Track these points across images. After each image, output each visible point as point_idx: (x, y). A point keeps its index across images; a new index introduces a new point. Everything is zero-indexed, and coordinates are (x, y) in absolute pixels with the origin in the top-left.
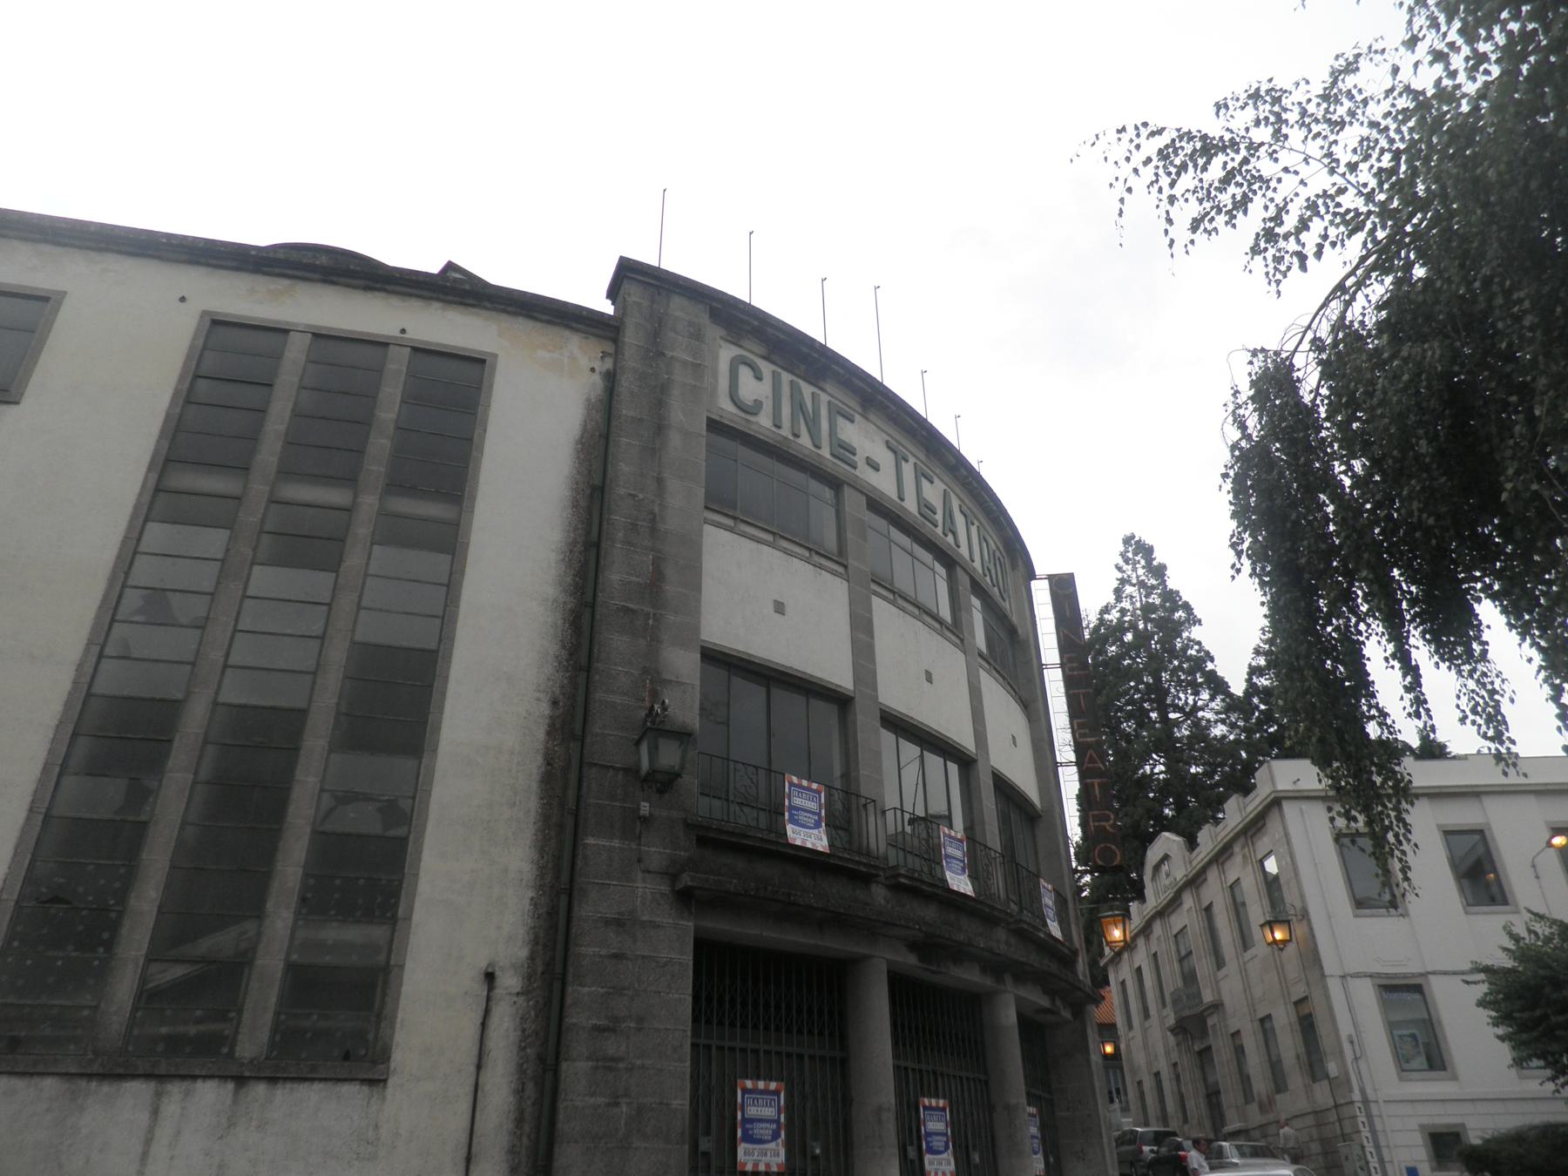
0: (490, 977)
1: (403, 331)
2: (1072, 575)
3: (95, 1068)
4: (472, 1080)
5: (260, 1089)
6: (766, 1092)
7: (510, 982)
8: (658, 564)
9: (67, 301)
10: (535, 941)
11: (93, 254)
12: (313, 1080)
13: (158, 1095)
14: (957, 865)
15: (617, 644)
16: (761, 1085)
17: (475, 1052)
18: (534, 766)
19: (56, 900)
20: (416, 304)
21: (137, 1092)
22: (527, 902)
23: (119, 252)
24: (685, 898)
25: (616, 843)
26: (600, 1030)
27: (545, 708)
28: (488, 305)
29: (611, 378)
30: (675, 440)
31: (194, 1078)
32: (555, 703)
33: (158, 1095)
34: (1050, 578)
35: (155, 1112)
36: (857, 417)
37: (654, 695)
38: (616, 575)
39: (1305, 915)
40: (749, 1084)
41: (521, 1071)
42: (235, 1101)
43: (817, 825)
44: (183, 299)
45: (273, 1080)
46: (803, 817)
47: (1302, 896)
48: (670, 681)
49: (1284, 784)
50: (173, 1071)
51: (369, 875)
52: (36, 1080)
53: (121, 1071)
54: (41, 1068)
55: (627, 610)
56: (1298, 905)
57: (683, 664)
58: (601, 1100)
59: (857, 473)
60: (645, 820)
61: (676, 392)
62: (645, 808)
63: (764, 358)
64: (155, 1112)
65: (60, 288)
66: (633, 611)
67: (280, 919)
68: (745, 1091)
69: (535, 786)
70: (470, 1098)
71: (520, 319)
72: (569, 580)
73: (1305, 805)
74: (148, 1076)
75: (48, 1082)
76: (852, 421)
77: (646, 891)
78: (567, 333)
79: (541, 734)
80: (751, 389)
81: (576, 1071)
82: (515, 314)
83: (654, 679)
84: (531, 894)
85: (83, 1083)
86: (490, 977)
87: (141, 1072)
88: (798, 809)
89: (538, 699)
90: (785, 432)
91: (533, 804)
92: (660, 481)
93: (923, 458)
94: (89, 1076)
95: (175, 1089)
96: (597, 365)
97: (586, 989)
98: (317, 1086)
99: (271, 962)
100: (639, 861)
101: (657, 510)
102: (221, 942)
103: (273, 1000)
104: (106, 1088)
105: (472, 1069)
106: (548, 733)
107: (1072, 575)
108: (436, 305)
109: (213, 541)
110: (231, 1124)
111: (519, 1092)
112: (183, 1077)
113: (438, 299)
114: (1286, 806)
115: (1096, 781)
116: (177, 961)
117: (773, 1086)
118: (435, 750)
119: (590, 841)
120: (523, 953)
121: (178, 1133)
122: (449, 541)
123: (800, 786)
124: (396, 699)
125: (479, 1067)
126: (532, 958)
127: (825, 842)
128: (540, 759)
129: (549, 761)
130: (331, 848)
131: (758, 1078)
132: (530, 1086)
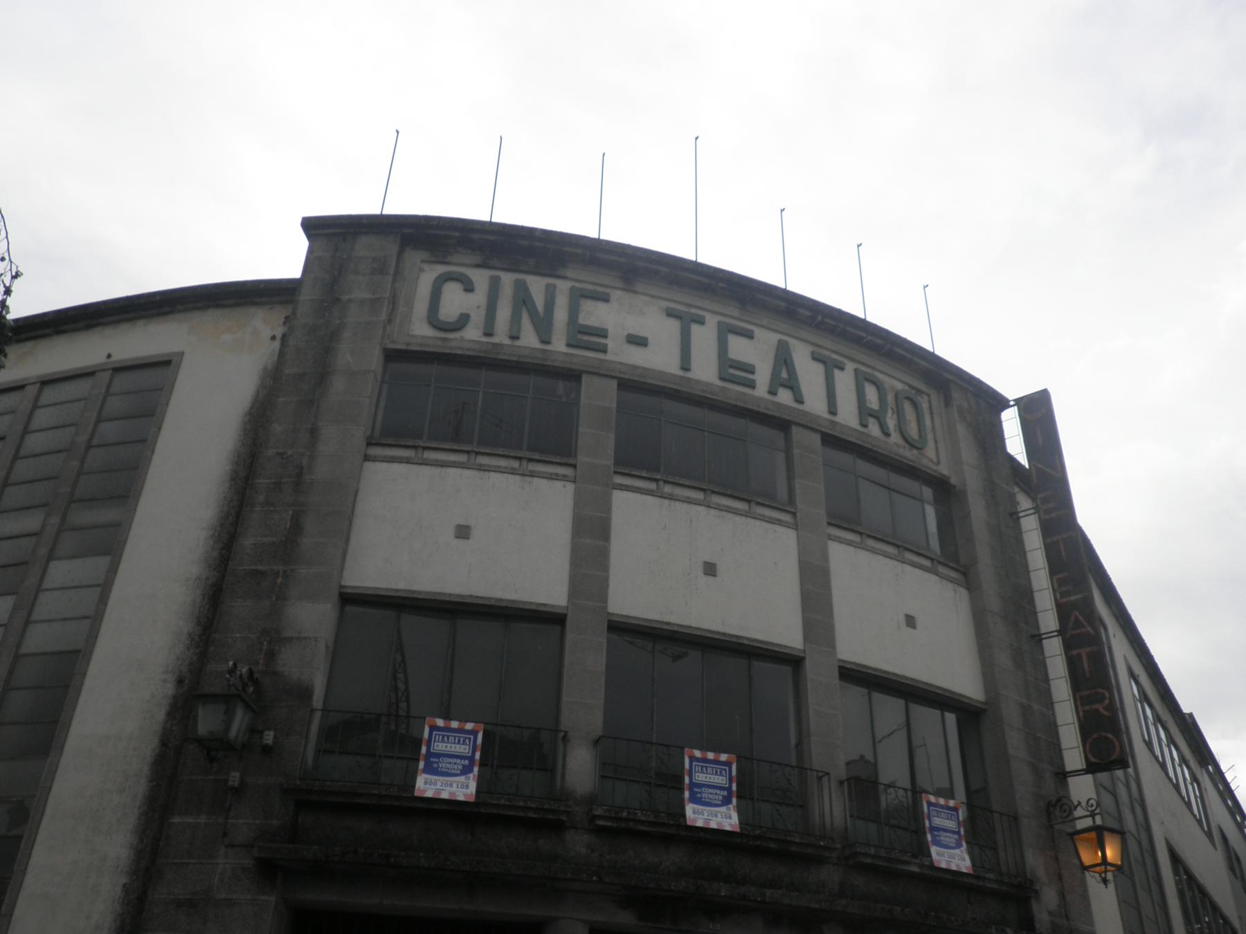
9: (186, 357)
14: (950, 839)
15: (240, 608)
18: (149, 748)
22: (119, 889)
24: (268, 870)
27: (170, 689)
28: (180, 307)
30: (338, 384)
32: (180, 681)
34: (1018, 402)
36: (616, 295)
43: (726, 801)
46: (707, 794)
48: (291, 639)
57: (312, 617)
59: (609, 357)
60: (238, 791)
62: (235, 778)
63: (478, 266)
65: (176, 350)
66: (262, 573)
69: (146, 769)
72: (215, 554)
76: (605, 299)
78: (253, 310)
79: (161, 715)
80: (454, 301)
82: (205, 308)
83: (273, 639)
84: (124, 880)
88: (701, 786)
89: (165, 681)
90: (501, 337)
91: (141, 788)
92: (314, 432)
93: (736, 313)
100: (225, 835)
101: (305, 462)
106: (169, 714)
108: (141, 323)
118: (62, 747)
119: (176, 820)
122: (110, 544)
123: (705, 760)
127: (968, 862)
128: (155, 742)
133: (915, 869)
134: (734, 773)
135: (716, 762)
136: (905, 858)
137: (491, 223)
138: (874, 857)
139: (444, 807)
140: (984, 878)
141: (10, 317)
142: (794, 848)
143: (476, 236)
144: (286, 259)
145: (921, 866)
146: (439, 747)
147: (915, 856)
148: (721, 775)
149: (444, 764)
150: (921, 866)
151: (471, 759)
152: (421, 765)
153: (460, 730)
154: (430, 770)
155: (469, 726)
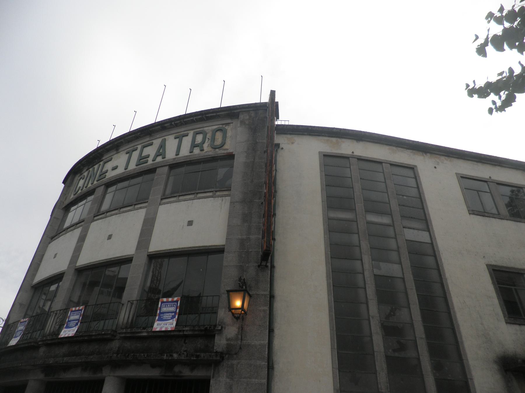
133: (145, 334)
134: (179, 305)
135: (167, 302)
136: (140, 330)
137: (221, 108)
138: (125, 333)
139: (163, 334)
140: (184, 331)
141: (278, 123)
142: (93, 337)
143: (108, 147)
144: (276, 101)
145: (148, 332)
146: (164, 309)
147: (144, 328)
148: (173, 306)
149: (165, 316)
150: (148, 332)
151: (175, 312)
152: (157, 318)
153: (172, 301)
154: (160, 319)
155: (175, 299)
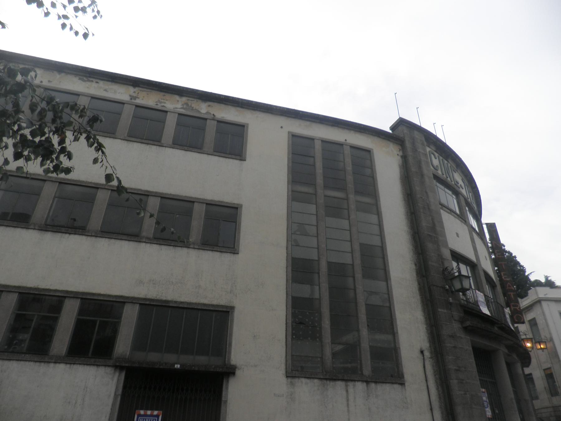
0: (422, 352)
1: (346, 140)
2: (494, 224)
3: (328, 377)
4: (425, 385)
5: (373, 385)
6: (152, 415)
7: (427, 354)
8: (433, 219)
10: (430, 342)
11: (252, 111)
12: (386, 383)
13: (347, 386)
16: (149, 412)
17: (424, 376)
19: (301, 323)
20: (346, 131)
21: (340, 385)
23: (260, 111)
25: (445, 311)
26: (457, 370)
27: (413, 267)
29: (404, 158)
30: (427, 180)
31: (355, 381)
32: (416, 265)
33: (347, 386)
35: (347, 391)
37: (443, 263)
38: (424, 223)
39: (551, 340)
40: (142, 412)
41: (436, 382)
42: (368, 389)
44: (282, 127)
45: (376, 382)
47: (550, 334)
49: (541, 296)
50: (349, 379)
51: (383, 319)
52: (312, 380)
53: (335, 378)
54: (313, 376)
55: (430, 235)
56: (548, 336)
58: (462, 393)
61: (423, 163)
64: (347, 391)
67: (364, 332)
68: (139, 415)
69: (418, 291)
70: (426, 390)
71: (376, 137)
73: (549, 303)
74: (342, 380)
75: (316, 381)
77: (456, 326)
81: (454, 383)
85: (325, 381)
86: (422, 352)
87: (340, 378)
92: (426, 192)
94: (326, 379)
95: (351, 384)
96: (398, 153)
97: (450, 357)
98: (388, 385)
99: (365, 345)
102: (349, 338)
103: (369, 357)
104: (332, 383)
105: (425, 381)
107: (494, 224)
108: (352, 132)
109: (312, 208)
110: (369, 396)
111: (437, 389)
112: (352, 381)
113: (353, 130)
114: (544, 304)
115: (512, 293)
116: (339, 344)
117: (156, 413)
120: (428, 345)
121: (355, 398)
124: (374, 261)
125: (426, 381)
126: (430, 346)
129: (419, 284)
130: (371, 309)
131: (147, 409)
132: (440, 387)
